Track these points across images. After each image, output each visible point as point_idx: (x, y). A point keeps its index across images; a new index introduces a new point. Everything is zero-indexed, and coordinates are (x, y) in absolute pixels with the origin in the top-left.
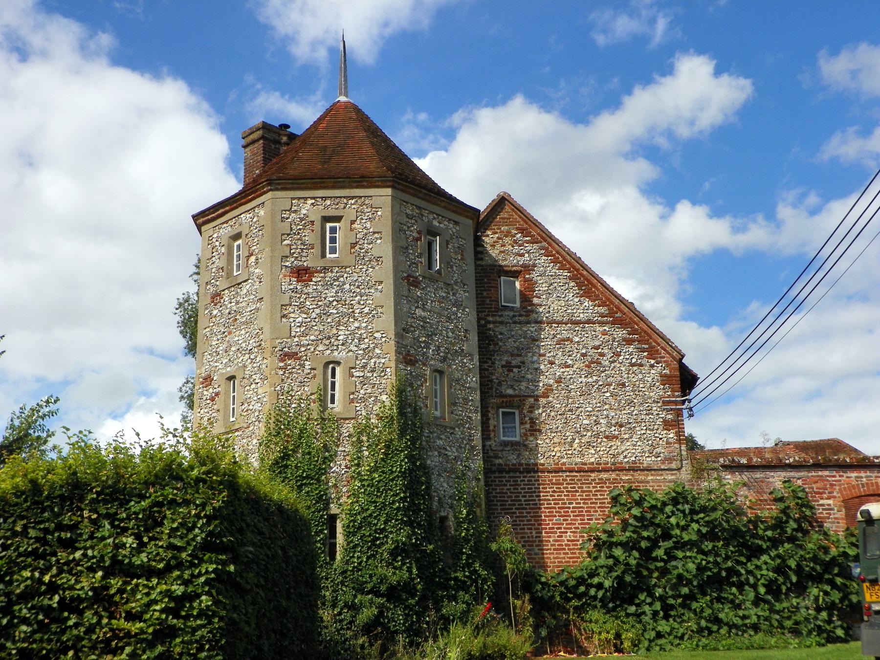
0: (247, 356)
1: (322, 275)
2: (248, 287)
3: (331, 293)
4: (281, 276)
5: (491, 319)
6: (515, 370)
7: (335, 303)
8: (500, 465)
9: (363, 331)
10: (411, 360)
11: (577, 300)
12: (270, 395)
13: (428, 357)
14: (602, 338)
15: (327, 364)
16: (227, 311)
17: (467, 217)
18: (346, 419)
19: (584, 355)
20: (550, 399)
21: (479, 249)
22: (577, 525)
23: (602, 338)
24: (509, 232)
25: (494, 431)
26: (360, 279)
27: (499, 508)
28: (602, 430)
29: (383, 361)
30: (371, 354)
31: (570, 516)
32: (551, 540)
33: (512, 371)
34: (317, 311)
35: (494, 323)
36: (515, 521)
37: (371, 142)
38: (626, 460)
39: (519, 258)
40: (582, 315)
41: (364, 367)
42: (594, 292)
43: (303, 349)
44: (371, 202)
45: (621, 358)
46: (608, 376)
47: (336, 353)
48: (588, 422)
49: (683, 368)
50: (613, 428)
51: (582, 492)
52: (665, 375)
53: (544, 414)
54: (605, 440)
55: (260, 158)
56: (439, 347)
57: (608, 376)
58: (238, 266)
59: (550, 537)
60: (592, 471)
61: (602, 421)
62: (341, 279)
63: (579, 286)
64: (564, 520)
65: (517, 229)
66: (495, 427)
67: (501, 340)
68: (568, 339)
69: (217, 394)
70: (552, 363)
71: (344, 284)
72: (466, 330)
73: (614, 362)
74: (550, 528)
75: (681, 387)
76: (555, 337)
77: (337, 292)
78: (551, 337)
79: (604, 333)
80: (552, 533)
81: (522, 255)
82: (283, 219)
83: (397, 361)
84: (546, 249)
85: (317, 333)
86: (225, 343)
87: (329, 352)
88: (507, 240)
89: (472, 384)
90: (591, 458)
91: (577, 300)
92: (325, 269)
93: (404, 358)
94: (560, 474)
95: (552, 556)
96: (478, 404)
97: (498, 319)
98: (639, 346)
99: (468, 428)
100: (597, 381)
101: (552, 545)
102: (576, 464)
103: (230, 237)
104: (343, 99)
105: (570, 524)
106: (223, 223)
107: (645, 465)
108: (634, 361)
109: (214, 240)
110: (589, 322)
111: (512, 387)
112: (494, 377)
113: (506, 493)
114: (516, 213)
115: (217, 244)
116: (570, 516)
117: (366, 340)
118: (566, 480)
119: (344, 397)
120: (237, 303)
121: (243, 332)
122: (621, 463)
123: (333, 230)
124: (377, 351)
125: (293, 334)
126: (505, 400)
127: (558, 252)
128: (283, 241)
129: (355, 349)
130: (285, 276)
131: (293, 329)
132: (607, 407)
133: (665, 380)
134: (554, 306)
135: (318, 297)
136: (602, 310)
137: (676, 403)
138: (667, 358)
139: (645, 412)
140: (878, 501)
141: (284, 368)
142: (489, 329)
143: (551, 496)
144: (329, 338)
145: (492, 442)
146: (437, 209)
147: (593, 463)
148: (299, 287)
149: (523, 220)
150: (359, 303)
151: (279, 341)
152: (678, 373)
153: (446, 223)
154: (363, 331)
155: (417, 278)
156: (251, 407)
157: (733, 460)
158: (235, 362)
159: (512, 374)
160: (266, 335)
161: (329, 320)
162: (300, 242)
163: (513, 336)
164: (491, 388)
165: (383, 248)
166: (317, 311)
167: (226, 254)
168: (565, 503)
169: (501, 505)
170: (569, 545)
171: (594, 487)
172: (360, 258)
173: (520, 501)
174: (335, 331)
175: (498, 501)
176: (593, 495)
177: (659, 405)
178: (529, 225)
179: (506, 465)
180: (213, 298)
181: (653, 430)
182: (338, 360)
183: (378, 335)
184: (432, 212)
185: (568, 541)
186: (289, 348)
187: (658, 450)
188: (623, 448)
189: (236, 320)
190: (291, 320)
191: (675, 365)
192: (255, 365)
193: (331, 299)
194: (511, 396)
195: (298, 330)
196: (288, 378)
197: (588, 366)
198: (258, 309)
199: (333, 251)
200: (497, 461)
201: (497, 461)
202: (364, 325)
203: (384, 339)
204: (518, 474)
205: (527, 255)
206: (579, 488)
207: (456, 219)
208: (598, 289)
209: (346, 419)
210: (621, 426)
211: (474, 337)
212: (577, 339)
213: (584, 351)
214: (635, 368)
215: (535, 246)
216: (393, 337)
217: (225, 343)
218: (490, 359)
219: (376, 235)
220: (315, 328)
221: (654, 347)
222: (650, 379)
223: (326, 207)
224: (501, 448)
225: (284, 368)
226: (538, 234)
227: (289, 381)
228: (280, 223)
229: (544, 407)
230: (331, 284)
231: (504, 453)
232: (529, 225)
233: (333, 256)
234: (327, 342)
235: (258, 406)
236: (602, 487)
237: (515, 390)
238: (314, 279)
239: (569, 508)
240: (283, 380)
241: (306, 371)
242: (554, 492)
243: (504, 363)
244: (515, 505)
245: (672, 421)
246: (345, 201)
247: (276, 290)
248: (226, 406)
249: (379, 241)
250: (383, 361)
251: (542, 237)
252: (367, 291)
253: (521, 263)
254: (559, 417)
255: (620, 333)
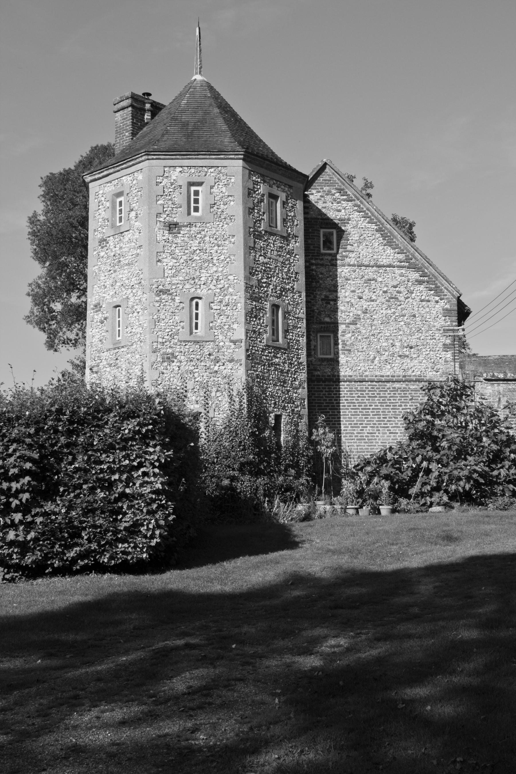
0: (130, 290)
1: (188, 229)
2: (129, 236)
3: (195, 244)
4: (156, 229)
5: (314, 262)
6: (332, 303)
7: (198, 251)
8: (318, 376)
9: (220, 274)
10: (256, 297)
11: (381, 248)
12: (149, 322)
13: (268, 294)
14: (399, 279)
15: (192, 299)
16: (113, 254)
17: (299, 182)
18: (207, 342)
19: (385, 292)
20: (358, 326)
21: (307, 205)
22: (375, 422)
23: (399, 279)
24: (329, 192)
25: (314, 350)
26: (217, 233)
27: (317, 408)
28: (397, 350)
29: (235, 297)
30: (225, 292)
31: (369, 415)
32: (355, 432)
33: (329, 303)
34: (185, 257)
35: (316, 265)
36: (329, 418)
37: (224, 118)
38: (414, 374)
39: (337, 213)
40: (384, 261)
41: (221, 302)
42: (395, 242)
43: (174, 287)
44: (226, 171)
45: (413, 295)
46: (403, 309)
47: (199, 291)
48: (386, 344)
49: (461, 305)
50: (405, 349)
51: (380, 397)
52: (447, 309)
53: (353, 338)
54: (398, 358)
55: (129, 122)
56: (276, 287)
57: (403, 309)
58: (121, 218)
59: (354, 430)
60: (388, 382)
61: (397, 344)
62: (203, 233)
63: (384, 237)
64: (365, 418)
65: (336, 189)
66: (315, 346)
67: (321, 279)
68: (374, 279)
69: (106, 319)
70: (360, 298)
71: (205, 236)
72: (297, 273)
73: (408, 298)
74: (355, 424)
75: (458, 319)
76: (363, 277)
77: (199, 243)
78: (360, 277)
79: (402, 275)
80: (356, 427)
81: (339, 211)
82: (157, 184)
83: (246, 298)
84: (359, 206)
85: (184, 275)
86: (112, 279)
87: (193, 290)
88: (329, 198)
89: (301, 315)
90: (387, 371)
91: (381, 248)
92: (190, 225)
93: (251, 296)
94: (364, 383)
95: (355, 444)
96: (304, 330)
97: (319, 262)
98: (428, 286)
99: (297, 349)
100: (394, 313)
101: (356, 436)
102: (376, 376)
103: (114, 195)
104: (198, 77)
105: (370, 421)
106: (107, 183)
107: (428, 378)
108: (423, 298)
109: (100, 196)
110: (390, 266)
111: (329, 316)
112: (315, 308)
113: (322, 397)
114: (336, 176)
115: (103, 199)
116: (369, 415)
117: (222, 281)
118: (368, 388)
119: (206, 325)
120: (121, 248)
121: (126, 271)
122: (410, 376)
123: (196, 193)
124: (231, 290)
125: (166, 275)
126: (323, 326)
127: (368, 209)
128: (157, 201)
129: (213, 288)
130: (159, 229)
131: (166, 271)
132: (401, 333)
133: (447, 312)
134: (364, 252)
135: (184, 247)
136: (401, 257)
137: (453, 331)
138: (449, 296)
139: (429, 337)
140: (1, 612)
141: (160, 301)
142: (312, 270)
143: (357, 400)
144: (194, 279)
145: (313, 358)
146: (276, 176)
147: (388, 376)
148: (170, 238)
149: (341, 182)
150: (217, 252)
151: (154, 280)
152: (456, 308)
153: (283, 187)
154: (220, 274)
155: (260, 232)
156: (134, 330)
157: (494, 375)
158: (120, 294)
159: (329, 306)
160: (145, 275)
161: (193, 265)
162: (170, 202)
163: (331, 276)
164: (313, 317)
165: (236, 208)
166: (185, 257)
167: (110, 208)
168: (367, 406)
169: (318, 406)
170: (368, 436)
171: (389, 394)
172: (219, 217)
173: (333, 403)
174: (198, 273)
175: (316, 403)
176: (388, 400)
177: (441, 332)
178: (346, 187)
179: (323, 376)
180: (100, 242)
181: (435, 351)
182: (201, 296)
183: (231, 278)
184: (272, 179)
185: (368, 433)
186: (163, 286)
187: (438, 367)
188: (412, 365)
189: (120, 261)
190: (165, 264)
191: (455, 301)
192: (136, 298)
193: (195, 248)
194: (328, 323)
195: (170, 272)
196: (163, 309)
197: (388, 301)
198: (138, 255)
199: (196, 209)
200: (316, 373)
201: (316, 373)
202: (220, 269)
203: (235, 281)
204: (332, 383)
205: (343, 211)
206: (378, 394)
207: (290, 184)
208: (398, 240)
209: (207, 342)
210: (411, 348)
211: (302, 278)
212: (380, 279)
213: (385, 289)
214: (424, 303)
215: (350, 203)
216: (243, 279)
217: (112, 279)
218: (313, 294)
219: (230, 198)
220: (183, 271)
221: (439, 287)
222: (435, 312)
223: (191, 175)
224: (319, 363)
225: (160, 301)
226: (353, 194)
227: (164, 311)
228: (155, 186)
229: (353, 332)
230: (195, 236)
231: (322, 367)
232: (346, 187)
233: (196, 214)
234: (193, 282)
235: (139, 330)
236: (395, 394)
237: (331, 318)
238: (182, 232)
239: (369, 409)
240: (158, 310)
241: (176, 305)
242: (359, 397)
243: (323, 297)
244: (329, 406)
245: (450, 344)
246: (206, 169)
247: (152, 240)
248: (113, 328)
249: (232, 203)
250: (235, 297)
251: (356, 196)
252: (223, 242)
253: (338, 217)
254: (364, 340)
255: (414, 276)
